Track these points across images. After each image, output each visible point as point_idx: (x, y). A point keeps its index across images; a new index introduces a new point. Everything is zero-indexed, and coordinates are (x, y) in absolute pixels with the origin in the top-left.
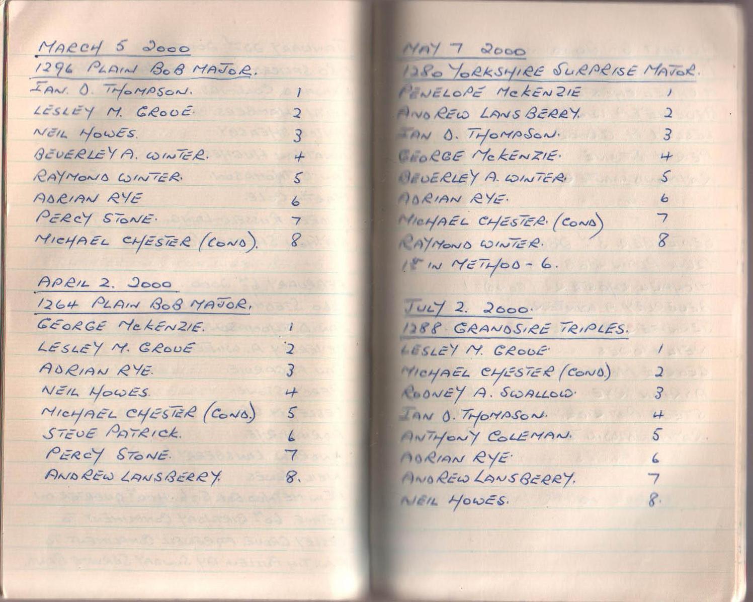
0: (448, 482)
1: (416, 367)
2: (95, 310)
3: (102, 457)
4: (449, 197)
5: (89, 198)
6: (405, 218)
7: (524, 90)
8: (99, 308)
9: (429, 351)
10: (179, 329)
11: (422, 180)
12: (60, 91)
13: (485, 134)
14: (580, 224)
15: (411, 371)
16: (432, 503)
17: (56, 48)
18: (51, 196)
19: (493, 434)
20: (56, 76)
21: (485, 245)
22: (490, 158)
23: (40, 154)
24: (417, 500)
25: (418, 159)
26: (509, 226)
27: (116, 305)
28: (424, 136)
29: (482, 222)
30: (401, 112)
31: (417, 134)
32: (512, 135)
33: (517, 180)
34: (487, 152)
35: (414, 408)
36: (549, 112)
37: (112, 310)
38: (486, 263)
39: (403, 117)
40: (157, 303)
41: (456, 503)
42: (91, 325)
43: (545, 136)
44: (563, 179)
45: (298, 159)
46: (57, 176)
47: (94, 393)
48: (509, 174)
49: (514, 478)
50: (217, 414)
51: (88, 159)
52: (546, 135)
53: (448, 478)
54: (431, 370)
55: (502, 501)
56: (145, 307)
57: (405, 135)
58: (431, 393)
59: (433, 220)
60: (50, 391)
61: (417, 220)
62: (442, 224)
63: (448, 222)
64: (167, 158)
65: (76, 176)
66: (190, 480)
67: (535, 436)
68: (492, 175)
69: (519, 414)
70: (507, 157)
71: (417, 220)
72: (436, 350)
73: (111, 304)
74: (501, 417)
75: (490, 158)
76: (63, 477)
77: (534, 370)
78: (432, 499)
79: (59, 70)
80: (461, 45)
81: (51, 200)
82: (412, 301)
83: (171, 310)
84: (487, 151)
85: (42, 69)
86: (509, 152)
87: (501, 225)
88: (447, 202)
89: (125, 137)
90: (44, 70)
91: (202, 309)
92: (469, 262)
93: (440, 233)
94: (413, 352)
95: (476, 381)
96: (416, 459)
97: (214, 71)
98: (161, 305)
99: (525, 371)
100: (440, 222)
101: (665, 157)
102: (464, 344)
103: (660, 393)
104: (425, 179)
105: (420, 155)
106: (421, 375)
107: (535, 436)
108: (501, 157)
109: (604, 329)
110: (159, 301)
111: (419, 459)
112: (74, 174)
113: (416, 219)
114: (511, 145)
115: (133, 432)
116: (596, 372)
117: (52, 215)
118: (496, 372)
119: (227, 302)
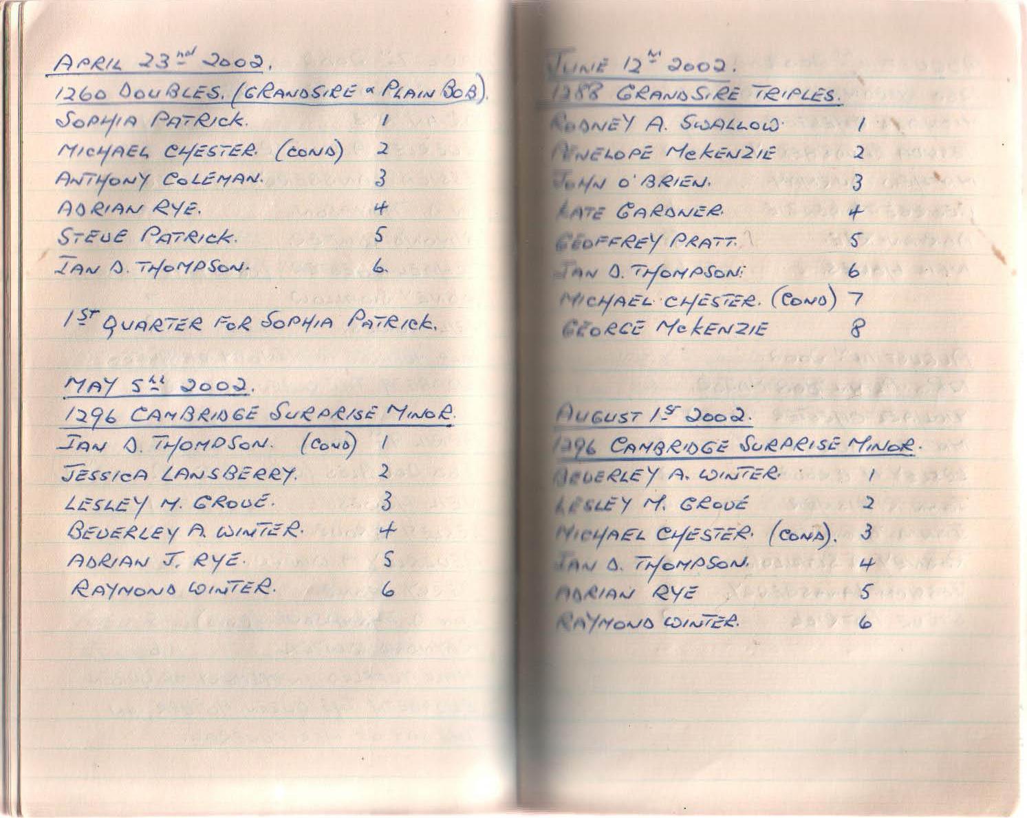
0: (636, 247)
4: (619, 533)
5: (130, 208)
6: (569, 297)
15: (568, 534)
18: (91, 558)
22: (689, 156)
23: (449, 87)
25: (581, 246)
28: (589, 273)
34: (683, 149)
35: (574, 262)
39: (568, 304)
41: (652, 276)
43: (802, 538)
46: (107, 589)
53: (636, 242)
55: (66, 238)
57: (566, 272)
58: (591, 125)
63: (627, 302)
66: (196, 328)
67: (168, 415)
68: (658, 121)
69: (713, 270)
70: (713, 154)
72: (602, 502)
74: (734, 101)
75: (689, 156)
80: (862, 294)
81: (92, 564)
82: (564, 555)
84: (683, 147)
89: (87, 481)
96: (574, 596)
101: (865, 565)
105: (583, 240)
107: (168, 415)
109: (809, 95)
110: (452, 84)
111: (577, 594)
114: (710, 315)
117: (86, 528)
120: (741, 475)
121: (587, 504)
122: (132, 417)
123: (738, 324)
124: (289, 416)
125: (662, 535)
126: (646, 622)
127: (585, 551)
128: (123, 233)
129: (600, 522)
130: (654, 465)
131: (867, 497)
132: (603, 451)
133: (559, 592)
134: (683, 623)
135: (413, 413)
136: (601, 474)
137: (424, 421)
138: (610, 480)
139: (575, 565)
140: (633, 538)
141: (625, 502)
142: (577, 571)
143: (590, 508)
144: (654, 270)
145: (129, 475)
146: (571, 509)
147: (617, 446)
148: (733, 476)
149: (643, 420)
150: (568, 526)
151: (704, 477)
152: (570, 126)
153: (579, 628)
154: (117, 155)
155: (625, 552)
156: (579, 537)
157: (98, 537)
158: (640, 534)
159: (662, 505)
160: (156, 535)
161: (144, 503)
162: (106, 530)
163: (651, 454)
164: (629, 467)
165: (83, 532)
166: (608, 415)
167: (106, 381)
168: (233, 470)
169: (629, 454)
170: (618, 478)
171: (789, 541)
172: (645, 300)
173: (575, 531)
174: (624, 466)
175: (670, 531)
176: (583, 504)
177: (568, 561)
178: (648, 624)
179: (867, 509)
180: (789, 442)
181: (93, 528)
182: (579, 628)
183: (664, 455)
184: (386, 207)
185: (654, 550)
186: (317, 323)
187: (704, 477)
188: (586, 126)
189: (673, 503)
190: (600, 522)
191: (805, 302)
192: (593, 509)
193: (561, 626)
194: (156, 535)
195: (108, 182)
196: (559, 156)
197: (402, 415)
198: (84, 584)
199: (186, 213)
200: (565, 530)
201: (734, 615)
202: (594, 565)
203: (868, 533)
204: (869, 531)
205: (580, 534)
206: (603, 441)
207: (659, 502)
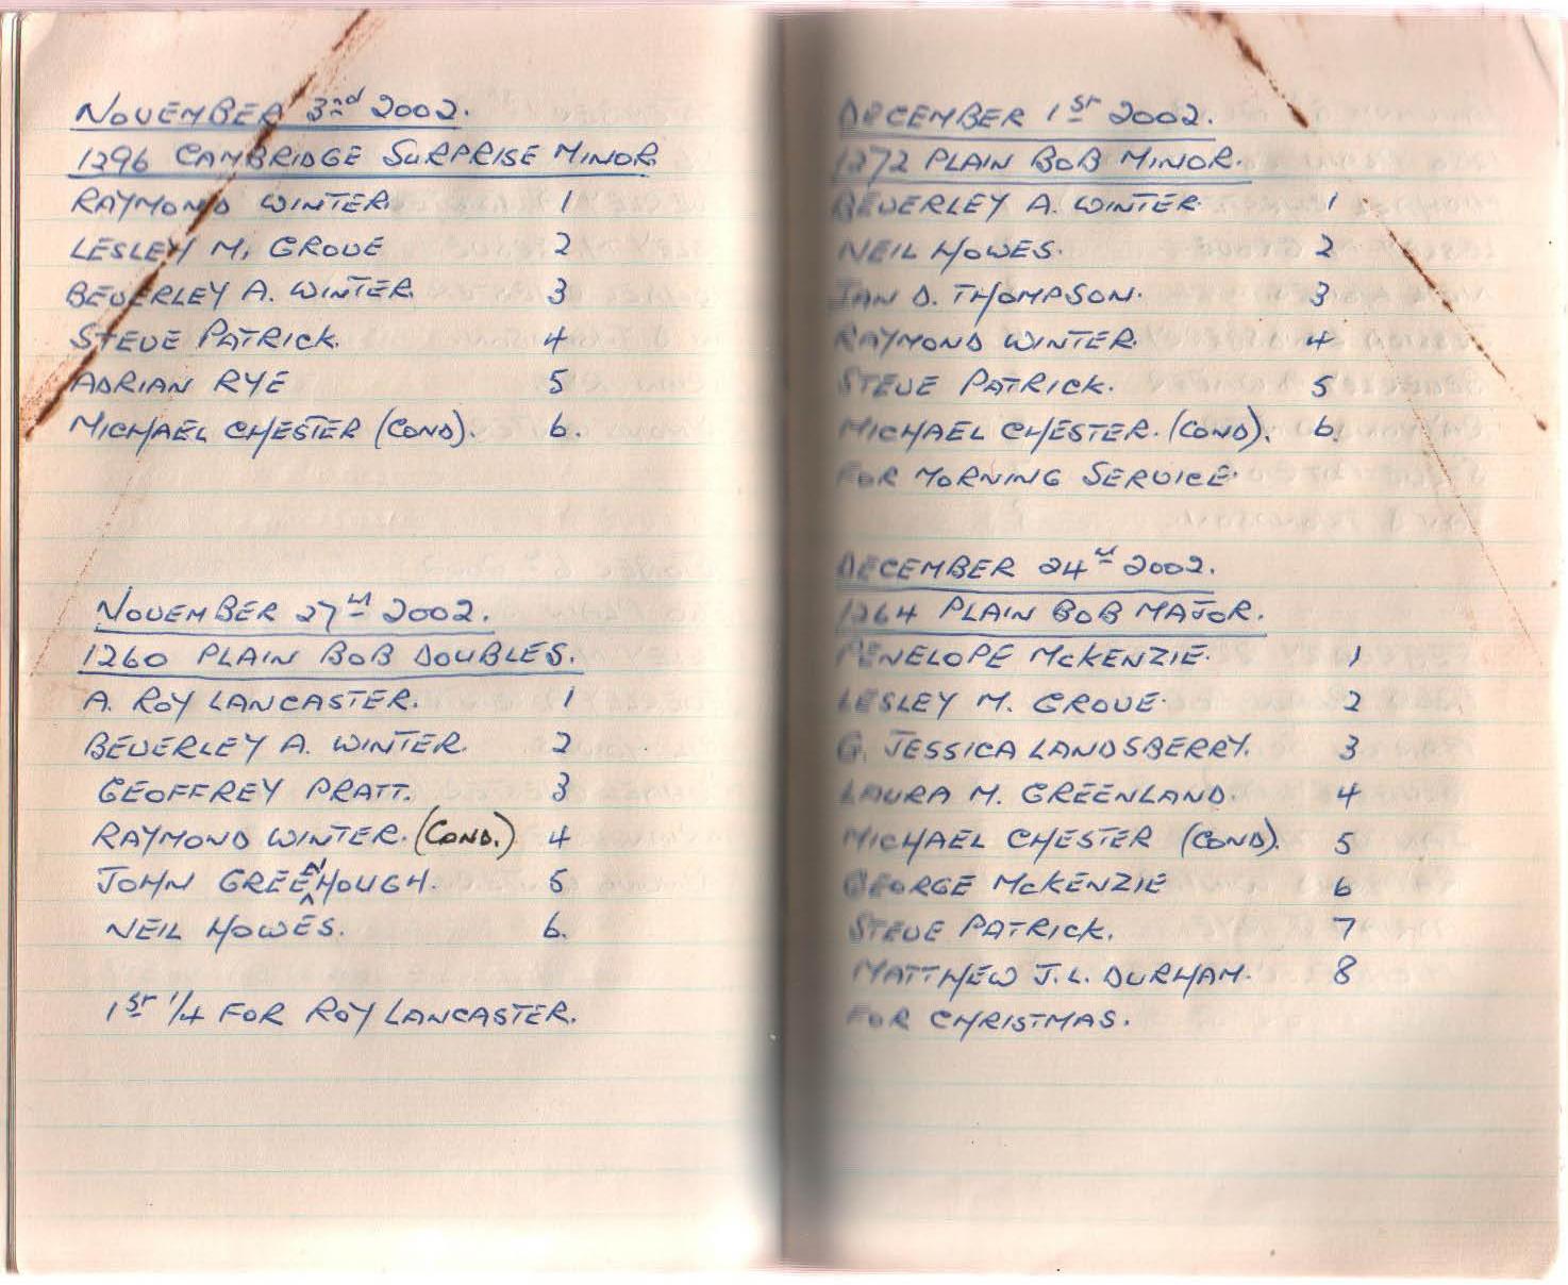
2: (201, 670)
3: (192, 889)
6: (854, 833)
8: (210, 666)
12: (283, 660)
14: (1111, 299)
15: (862, 839)
17: (176, 1000)
20: (269, 793)
21: (344, 746)
26: (1066, 440)
27: (241, 658)
31: (866, 299)
32: (1041, 296)
42: (113, 788)
44: (1130, 344)
45: (1082, 568)
47: (945, 252)
49: (1089, 840)
52: (1114, 295)
59: (914, 429)
60: (112, 613)
61: (878, 430)
62: (932, 437)
63: (946, 432)
64: (304, 208)
65: (156, 204)
69: (1083, 291)
71: (878, 430)
73: (233, 657)
76: (380, 747)
79: (143, 157)
82: (850, 284)
85: (941, 969)
87: (1057, 845)
92: (277, 424)
93: (937, 864)
94: (859, 703)
95: (996, 860)
97: (316, 705)
99: (1096, 838)
100: (929, 431)
106: (882, 844)
112: (152, 200)
113: (876, 428)
116: (1248, 840)
118: (1183, 973)
120: (1136, 207)
121: (885, 699)
123: (1100, 830)
125: (1017, 840)
129: (910, 411)
131: (1351, 692)
135: (591, 156)
137: (611, 167)
139: (864, 299)
140: (966, 844)
141: (943, 699)
142: (875, 349)
143: (889, 706)
145: (307, 338)
148: (1125, 207)
152: (876, 1019)
157: (130, 754)
158: (977, 430)
159: (1005, 703)
160: (195, 298)
161: (187, 249)
162: (146, 743)
165: (87, 295)
166: (905, 699)
167: (175, 699)
173: (871, 836)
175: (1029, 834)
176: (878, 700)
177: (852, 293)
179: (1350, 712)
181: (168, 739)
184: (568, 839)
188: (885, 433)
189: (1021, 700)
190: (910, 411)
191: (1214, 433)
193: (841, 347)
194: (195, 298)
195: (160, 207)
196: (851, 661)
197: (989, 799)
198: (111, 830)
200: (869, 965)
203: (560, 295)
204: (562, 291)
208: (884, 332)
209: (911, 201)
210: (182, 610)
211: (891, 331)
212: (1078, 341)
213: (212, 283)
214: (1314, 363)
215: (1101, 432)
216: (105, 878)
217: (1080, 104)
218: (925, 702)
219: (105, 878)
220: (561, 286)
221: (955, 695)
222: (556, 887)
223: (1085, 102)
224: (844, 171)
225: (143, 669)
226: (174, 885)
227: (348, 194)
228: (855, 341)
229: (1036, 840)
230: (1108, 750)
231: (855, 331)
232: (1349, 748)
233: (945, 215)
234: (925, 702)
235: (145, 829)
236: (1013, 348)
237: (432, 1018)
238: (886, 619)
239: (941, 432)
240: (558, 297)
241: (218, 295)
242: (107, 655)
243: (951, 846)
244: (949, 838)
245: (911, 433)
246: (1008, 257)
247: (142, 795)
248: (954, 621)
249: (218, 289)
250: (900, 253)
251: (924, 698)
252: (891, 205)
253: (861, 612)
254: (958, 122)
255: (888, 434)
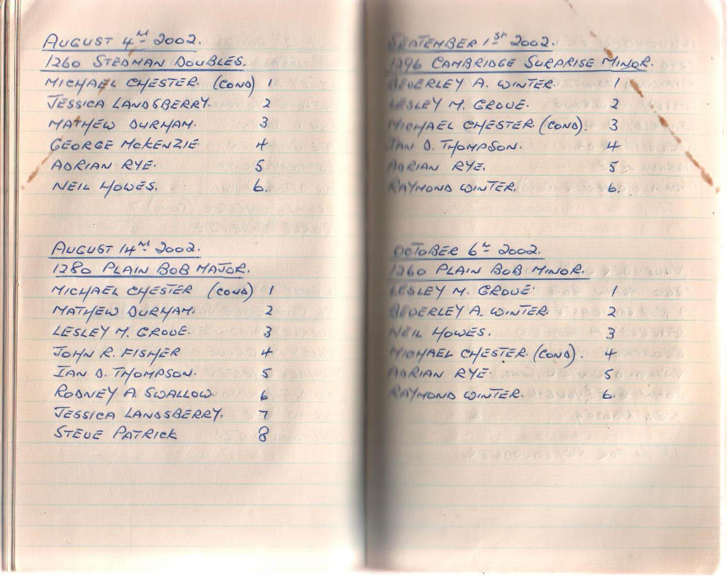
1: (405, 348)
7: (519, 352)
9: (80, 332)
10: (175, 146)
11: (410, 314)
13: (454, 146)
15: (398, 353)
16: (417, 335)
19: (437, 61)
20: (104, 331)
21: (502, 86)
24: (402, 331)
29: (464, 355)
30: (390, 165)
31: (401, 146)
32: (476, 148)
33: (503, 314)
36: (538, 310)
37: (455, 277)
38: (449, 143)
40: (468, 63)
48: (494, 307)
50: (225, 85)
51: (84, 190)
54: (417, 351)
56: (153, 271)
59: (422, 352)
62: (94, 168)
63: (101, 290)
73: (120, 270)
74: (82, 185)
77: (508, 351)
78: (417, 332)
83: (178, 274)
86: (153, 141)
88: (141, 123)
90: (53, 65)
91: (206, 273)
94: (423, 107)
98: (168, 270)
102: (450, 286)
103: (265, 122)
104: (413, 312)
108: (146, 145)
110: (166, 266)
115: (502, 350)
118: (142, 290)
119: (227, 266)
122: (148, 390)
124: (538, 64)
126: (446, 187)
127: (407, 137)
128: (100, 432)
130: (460, 77)
132: (426, 66)
133: (390, 165)
134: (473, 188)
136: (421, 81)
138: (428, 87)
139: (406, 394)
144: (129, 373)
146: (401, 314)
147: (438, 64)
149: (479, 46)
150: (397, 100)
151: (500, 85)
153: (402, 191)
154: (95, 293)
155: (436, 137)
156: (405, 127)
163: (461, 69)
164: (443, 78)
168: (437, 248)
169: (445, 69)
170: (499, 293)
171: (547, 358)
172: (107, 311)
174: (437, 78)
178: (448, 189)
180: (560, 62)
182: (402, 191)
183: (471, 69)
185: (459, 135)
186: (67, 290)
187: (500, 85)
188: (409, 354)
192: (172, 376)
199: (58, 106)
201: (513, 183)
202: (413, 146)
205: (405, 125)
206: (426, 61)
207: (460, 104)
208: (410, 184)
209: (421, 81)
210: (508, 393)
211: (413, 183)
212: (498, 393)
213: (109, 388)
214: (610, 155)
215: (512, 125)
216: (52, 100)
217: (498, 36)
218: (430, 291)
219: (52, 100)
220: (265, 120)
221: (441, 100)
222: (259, 168)
223: (500, 35)
224: (395, 276)
225: (71, 68)
226: (552, 272)
227: (509, 348)
228: (398, 394)
229: (81, 293)
230: (145, 105)
231: (400, 389)
232: (267, 332)
233: (435, 89)
234: (430, 291)
235: (202, 99)
236: (501, 87)
237: (431, 167)
238: (413, 274)
239: (140, 415)
240: (264, 124)
241: (112, 394)
242: (62, 268)
243: (437, 356)
244: (408, 372)
245: (421, 354)
246: (465, 335)
247: (69, 147)
248: (443, 274)
249: (112, 390)
250: (420, 167)
251: (430, 289)
252: (414, 312)
253: (399, 63)
254: (446, 46)
255: (410, 355)
